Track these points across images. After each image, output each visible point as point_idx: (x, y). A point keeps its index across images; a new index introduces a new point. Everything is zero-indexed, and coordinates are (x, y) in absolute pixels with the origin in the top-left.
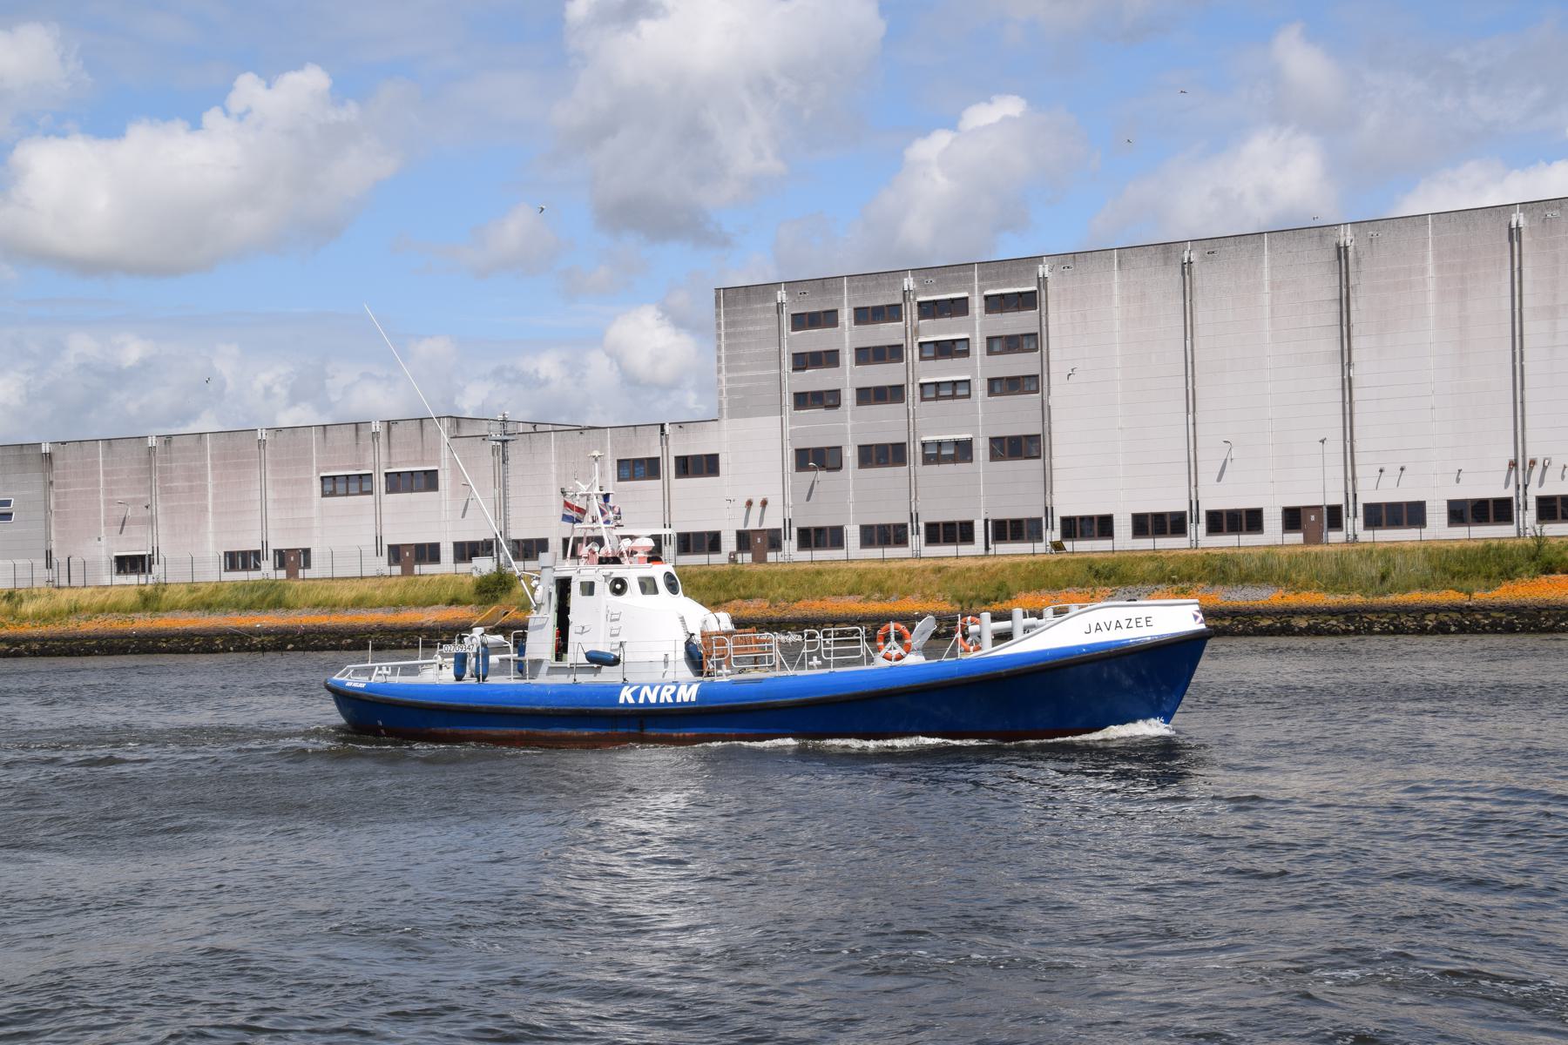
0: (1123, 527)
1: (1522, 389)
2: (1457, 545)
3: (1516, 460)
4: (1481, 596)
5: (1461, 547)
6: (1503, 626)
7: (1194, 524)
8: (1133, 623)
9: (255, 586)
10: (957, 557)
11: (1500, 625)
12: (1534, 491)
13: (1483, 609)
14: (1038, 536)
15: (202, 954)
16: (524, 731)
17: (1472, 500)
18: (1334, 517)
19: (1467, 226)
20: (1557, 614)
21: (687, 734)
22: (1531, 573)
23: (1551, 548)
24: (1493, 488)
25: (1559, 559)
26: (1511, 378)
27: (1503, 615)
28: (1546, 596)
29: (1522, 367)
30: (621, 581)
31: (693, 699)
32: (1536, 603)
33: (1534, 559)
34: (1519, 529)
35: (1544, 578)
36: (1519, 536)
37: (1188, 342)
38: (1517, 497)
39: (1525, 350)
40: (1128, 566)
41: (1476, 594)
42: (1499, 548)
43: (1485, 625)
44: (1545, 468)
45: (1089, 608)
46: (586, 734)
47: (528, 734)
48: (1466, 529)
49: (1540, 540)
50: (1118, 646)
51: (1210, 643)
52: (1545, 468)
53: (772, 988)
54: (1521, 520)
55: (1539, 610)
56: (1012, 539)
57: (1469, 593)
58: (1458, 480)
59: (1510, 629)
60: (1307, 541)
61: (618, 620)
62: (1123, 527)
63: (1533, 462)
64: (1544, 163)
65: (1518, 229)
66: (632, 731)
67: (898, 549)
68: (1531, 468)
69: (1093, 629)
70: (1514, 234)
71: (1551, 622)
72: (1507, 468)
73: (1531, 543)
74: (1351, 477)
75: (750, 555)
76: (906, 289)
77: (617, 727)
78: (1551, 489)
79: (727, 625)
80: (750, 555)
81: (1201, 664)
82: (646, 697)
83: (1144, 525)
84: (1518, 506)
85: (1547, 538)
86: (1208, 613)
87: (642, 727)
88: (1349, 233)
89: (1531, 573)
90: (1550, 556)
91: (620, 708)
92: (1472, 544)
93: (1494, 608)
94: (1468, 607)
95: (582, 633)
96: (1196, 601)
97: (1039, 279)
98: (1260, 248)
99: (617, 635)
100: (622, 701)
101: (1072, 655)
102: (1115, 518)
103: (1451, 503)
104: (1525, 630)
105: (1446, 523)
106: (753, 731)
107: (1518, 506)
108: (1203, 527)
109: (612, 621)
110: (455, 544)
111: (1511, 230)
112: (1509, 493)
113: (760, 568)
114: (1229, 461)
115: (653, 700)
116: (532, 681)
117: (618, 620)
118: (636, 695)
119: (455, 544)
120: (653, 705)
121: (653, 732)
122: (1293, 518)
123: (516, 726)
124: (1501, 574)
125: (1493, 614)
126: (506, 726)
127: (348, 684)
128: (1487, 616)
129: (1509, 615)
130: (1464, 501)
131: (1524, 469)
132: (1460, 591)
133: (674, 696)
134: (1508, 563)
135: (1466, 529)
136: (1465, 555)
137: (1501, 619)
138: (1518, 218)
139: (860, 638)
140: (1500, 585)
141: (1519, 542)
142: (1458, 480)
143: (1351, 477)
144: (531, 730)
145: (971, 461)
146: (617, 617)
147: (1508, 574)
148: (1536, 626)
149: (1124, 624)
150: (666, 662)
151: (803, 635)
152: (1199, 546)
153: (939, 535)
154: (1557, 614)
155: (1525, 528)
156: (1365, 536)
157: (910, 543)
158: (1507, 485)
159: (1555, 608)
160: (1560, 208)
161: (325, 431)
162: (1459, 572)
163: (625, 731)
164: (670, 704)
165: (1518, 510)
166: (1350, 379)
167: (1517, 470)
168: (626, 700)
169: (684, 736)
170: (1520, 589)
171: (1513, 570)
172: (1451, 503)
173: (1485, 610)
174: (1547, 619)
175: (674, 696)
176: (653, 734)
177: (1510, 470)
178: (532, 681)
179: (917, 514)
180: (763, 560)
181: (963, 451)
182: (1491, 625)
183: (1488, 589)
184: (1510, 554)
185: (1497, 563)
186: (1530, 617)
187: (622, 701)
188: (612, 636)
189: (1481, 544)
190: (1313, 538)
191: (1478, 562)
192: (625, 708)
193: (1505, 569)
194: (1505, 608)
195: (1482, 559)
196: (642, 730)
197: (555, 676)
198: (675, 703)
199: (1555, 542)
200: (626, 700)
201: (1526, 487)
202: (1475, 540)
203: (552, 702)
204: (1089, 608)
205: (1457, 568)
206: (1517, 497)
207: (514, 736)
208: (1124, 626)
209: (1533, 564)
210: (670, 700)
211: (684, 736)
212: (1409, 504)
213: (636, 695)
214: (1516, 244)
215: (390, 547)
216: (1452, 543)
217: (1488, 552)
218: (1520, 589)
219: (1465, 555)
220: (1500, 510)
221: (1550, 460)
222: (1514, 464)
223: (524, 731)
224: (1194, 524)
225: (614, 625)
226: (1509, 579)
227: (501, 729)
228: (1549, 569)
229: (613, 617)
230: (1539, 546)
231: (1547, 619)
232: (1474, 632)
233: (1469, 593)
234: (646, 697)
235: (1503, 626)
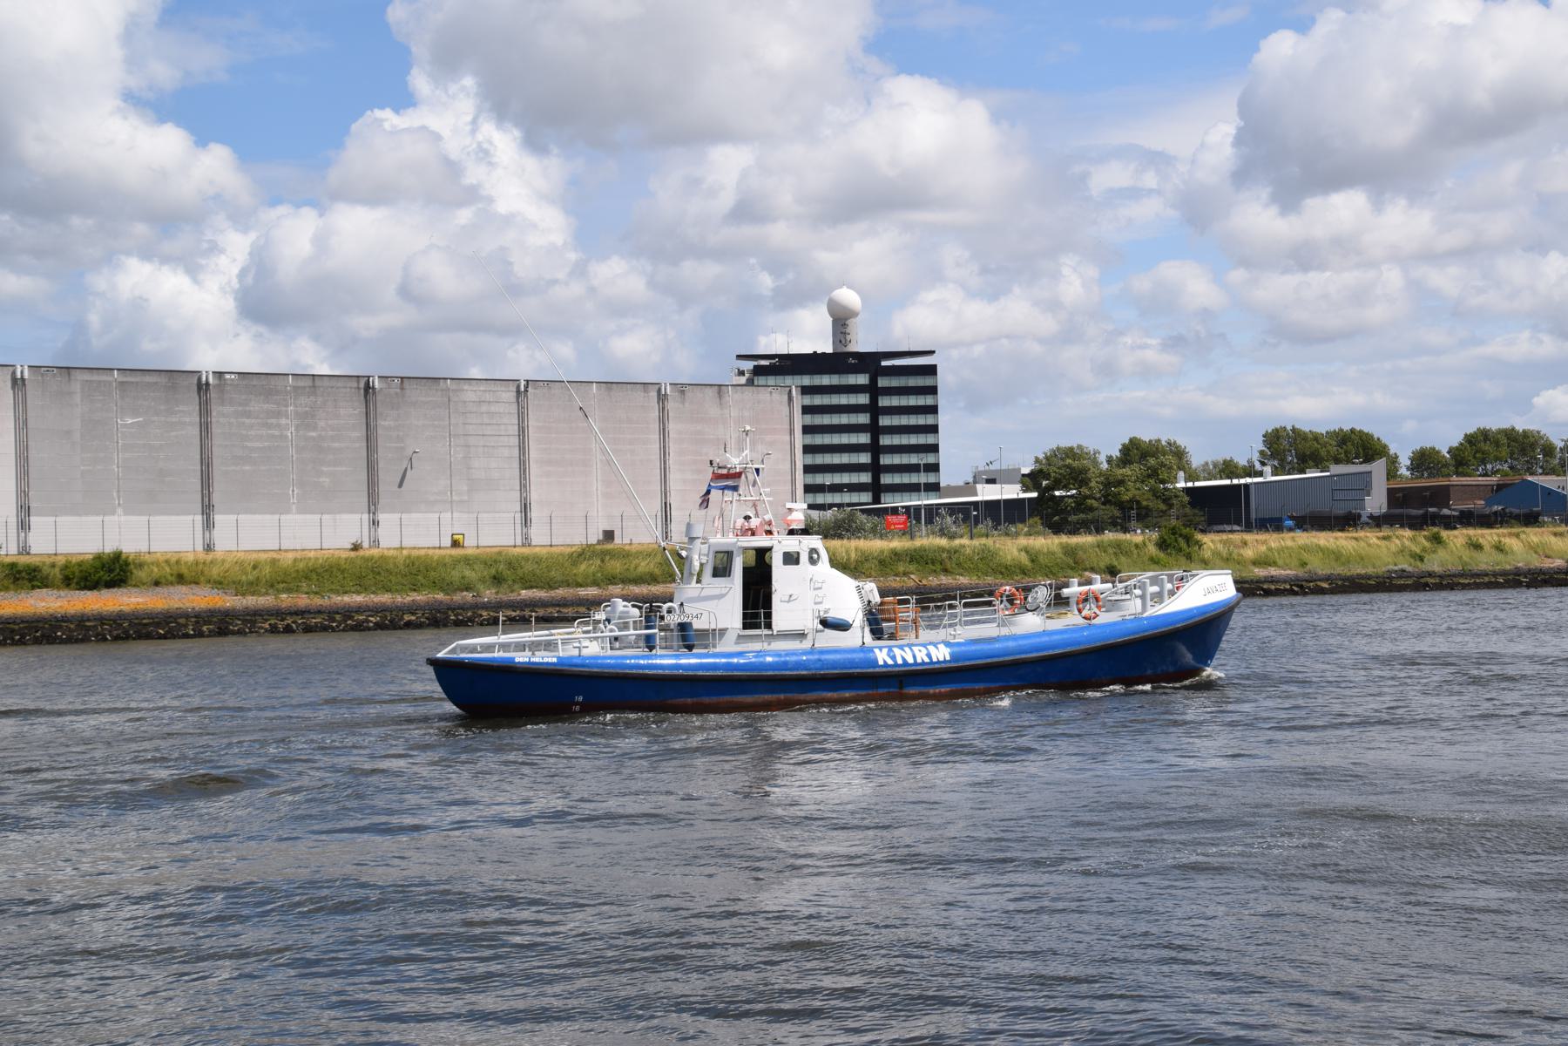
15: (1506, 1037)
16: (782, 696)
21: (943, 690)
46: (847, 695)
53: (1137, 881)
61: (820, 588)
64: (1265, 193)
81: (1233, 617)
88: (387, 423)
95: (789, 601)
101: (1205, 613)
106: (981, 686)
115: (911, 661)
117: (820, 588)
121: (912, 691)
123: (773, 692)
126: (762, 693)
127: (517, 660)
143: (666, 536)
146: (820, 585)
161: (314, 380)
163: (885, 690)
168: (885, 661)
188: (816, 603)
196: (901, 688)
198: (916, 663)
207: (771, 702)
223: (782, 696)
229: (816, 586)
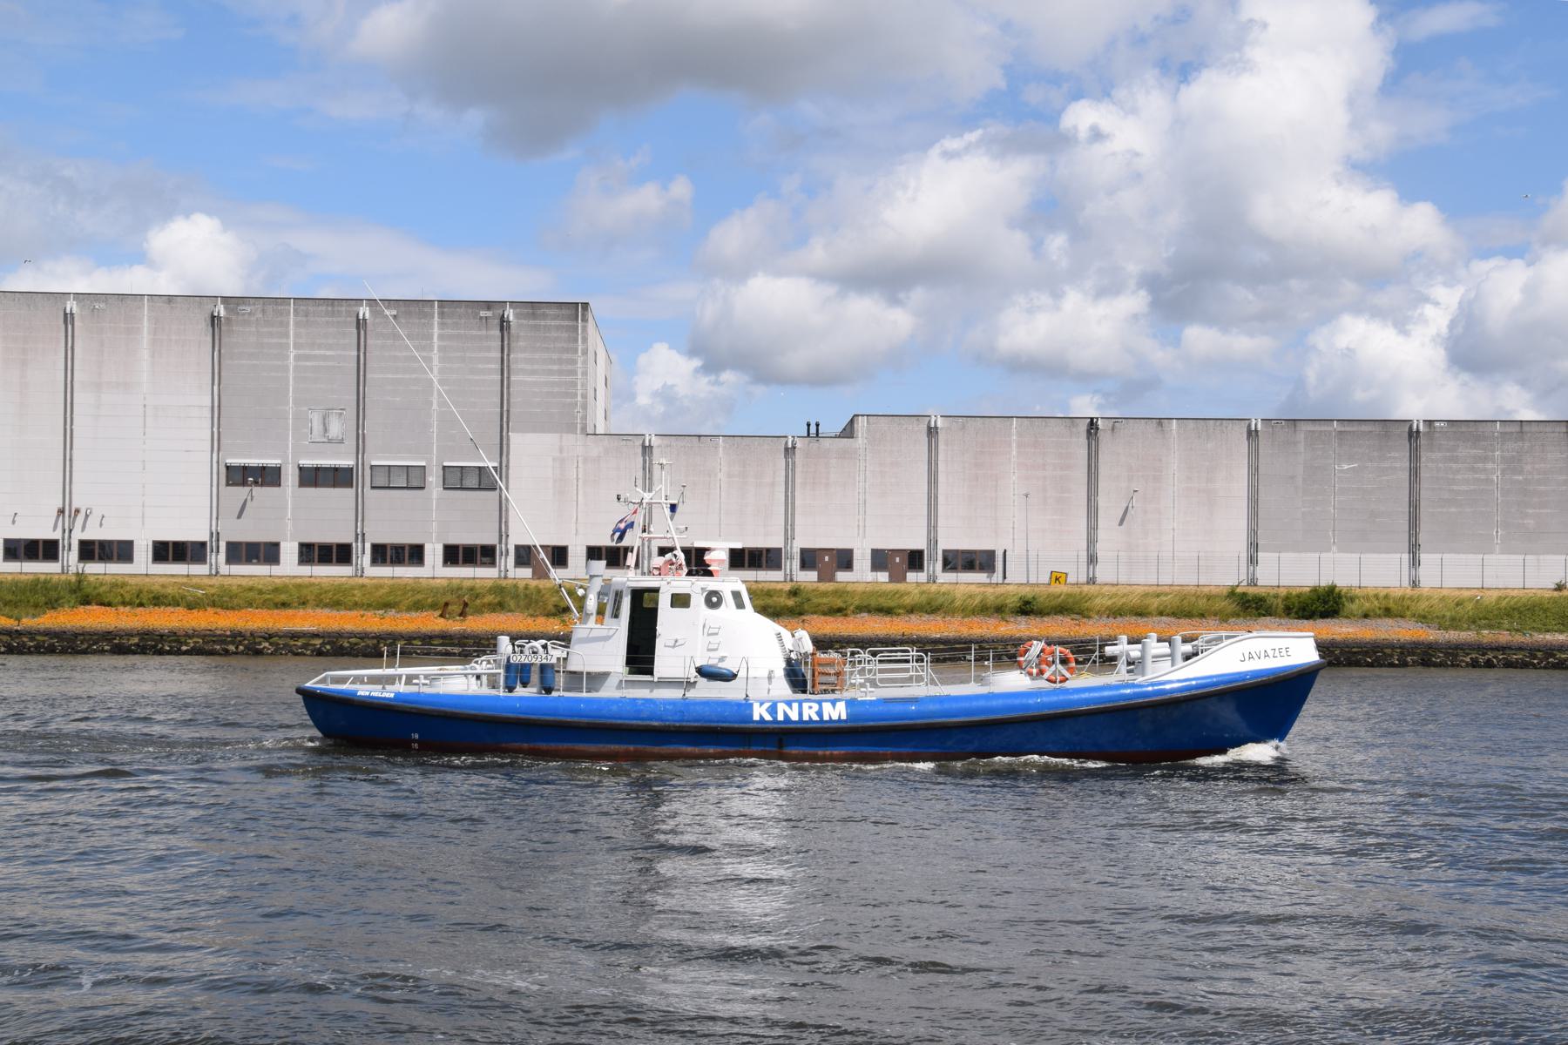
0: (142, 553)
1: (71, 448)
2: (10, 578)
3: (64, 508)
4: (29, 622)
5: (13, 580)
6: (46, 648)
7: (214, 554)
8: (1277, 654)
9: (414, 588)
10: (188, 576)
11: (43, 647)
12: (78, 535)
13: (30, 633)
14: (778, 566)
17: (25, 540)
18: (915, 559)
19: (29, 306)
20: (90, 639)
21: (835, 752)
22: (71, 604)
23: (89, 584)
24: (42, 530)
25: (95, 593)
26: (62, 438)
27: (46, 638)
28: (83, 624)
29: (72, 430)
30: (714, 593)
31: (844, 717)
32: (74, 629)
33: (75, 592)
34: (63, 567)
35: (81, 609)
36: (63, 573)
37: (216, 388)
38: (63, 539)
39: (74, 416)
40: (1194, 599)
41: (24, 620)
42: (46, 582)
43: (30, 647)
44: (87, 516)
45: (1240, 638)
47: (635, 751)
48: (19, 564)
49: (81, 577)
50: (1273, 674)
51: (1321, 673)
52: (87, 516)
54: (788, 567)
55: (76, 635)
56: (392, 562)
57: (18, 619)
58: (14, 522)
59: (51, 651)
60: (820, 579)
61: (717, 634)
62: (142, 553)
63: (77, 511)
65: (72, 314)
66: (768, 749)
67: (770, 573)
68: (76, 516)
69: (1247, 658)
70: (68, 318)
71: (85, 646)
72: (56, 514)
73: (73, 579)
74: (932, 528)
75: (887, 574)
76: (216, 314)
77: (750, 745)
78: (90, 535)
79: (808, 646)
80: (887, 574)
82: (786, 714)
83: (165, 551)
84: (64, 547)
85: (86, 576)
86: (1322, 647)
87: (781, 745)
89: (71, 604)
90: (89, 590)
91: (755, 725)
92: (23, 577)
93: (39, 633)
94: (17, 631)
95: (674, 647)
96: (1312, 634)
97: (358, 320)
98: (141, 308)
99: (716, 650)
100: (756, 717)
102: (135, 543)
103: (7, 541)
104: (63, 652)
105: (297, 562)
107: (64, 547)
108: (511, 559)
109: (709, 635)
110: (873, 550)
111: (66, 314)
112: (57, 535)
113: (542, 584)
114: (1130, 508)
116: (593, 695)
117: (717, 634)
118: (773, 710)
119: (873, 550)
120: (795, 722)
121: (794, 751)
122: (880, 559)
124: (46, 603)
125: (38, 638)
128: (32, 639)
129: (51, 638)
130: (18, 541)
131: (70, 516)
132: (10, 617)
133: (820, 713)
134: (54, 595)
135: (18, 564)
136: (16, 587)
137: (44, 642)
138: (71, 305)
139: (925, 664)
140: (45, 613)
141: (63, 577)
142: (14, 522)
143: (932, 528)
144: (640, 747)
145: (280, 485)
146: (716, 631)
147: (53, 604)
148: (73, 649)
149: (1271, 653)
150: (770, 678)
151: (844, 655)
152: (365, 575)
153: (44, 549)
154: (90, 639)
155: (68, 566)
156: (225, 569)
157: (926, 568)
158: (54, 530)
159: (90, 634)
160: (106, 302)
161: (1521, 426)
162: (11, 601)
164: (816, 722)
165: (63, 550)
166: (363, 434)
167: (64, 517)
168: (761, 716)
169: (832, 754)
170: (61, 617)
171: (56, 601)
172: (7, 541)
173: (31, 634)
174: (82, 643)
175: (820, 713)
176: (794, 752)
177: (58, 516)
178: (593, 695)
179: (364, 534)
180: (832, 579)
181: (312, 477)
182: (35, 647)
183: (34, 616)
184: (56, 587)
185: (46, 595)
186: (68, 640)
187: (756, 717)
189: (31, 577)
190: (897, 577)
191: (28, 593)
192: (759, 726)
193: (51, 600)
194: (48, 633)
195: (31, 590)
197: (631, 690)
199: (92, 579)
200: (761, 716)
201: (70, 531)
202: (26, 574)
203: (670, 718)
204: (1240, 638)
205: (9, 597)
206: (63, 539)
208: (1271, 655)
209: (74, 596)
210: (815, 718)
211: (832, 754)
212: (120, 542)
213: (773, 710)
214: (70, 327)
215: (517, 548)
216: (5, 576)
217: (37, 585)
218: (61, 617)
219: (16, 587)
220: (48, 550)
221: (91, 509)
222: (61, 511)
223: (631, 748)
224: (214, 554)
225: (711, 639)
226: (53, 608)
227: (601, 746)
228: (86, 601)
229: (711, 631)
230: (80, 582)
231: (82, 643)
232: (21, 653)
233: (18, 619)
234: (786, 714)
235: (46, 648)
